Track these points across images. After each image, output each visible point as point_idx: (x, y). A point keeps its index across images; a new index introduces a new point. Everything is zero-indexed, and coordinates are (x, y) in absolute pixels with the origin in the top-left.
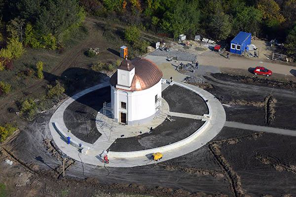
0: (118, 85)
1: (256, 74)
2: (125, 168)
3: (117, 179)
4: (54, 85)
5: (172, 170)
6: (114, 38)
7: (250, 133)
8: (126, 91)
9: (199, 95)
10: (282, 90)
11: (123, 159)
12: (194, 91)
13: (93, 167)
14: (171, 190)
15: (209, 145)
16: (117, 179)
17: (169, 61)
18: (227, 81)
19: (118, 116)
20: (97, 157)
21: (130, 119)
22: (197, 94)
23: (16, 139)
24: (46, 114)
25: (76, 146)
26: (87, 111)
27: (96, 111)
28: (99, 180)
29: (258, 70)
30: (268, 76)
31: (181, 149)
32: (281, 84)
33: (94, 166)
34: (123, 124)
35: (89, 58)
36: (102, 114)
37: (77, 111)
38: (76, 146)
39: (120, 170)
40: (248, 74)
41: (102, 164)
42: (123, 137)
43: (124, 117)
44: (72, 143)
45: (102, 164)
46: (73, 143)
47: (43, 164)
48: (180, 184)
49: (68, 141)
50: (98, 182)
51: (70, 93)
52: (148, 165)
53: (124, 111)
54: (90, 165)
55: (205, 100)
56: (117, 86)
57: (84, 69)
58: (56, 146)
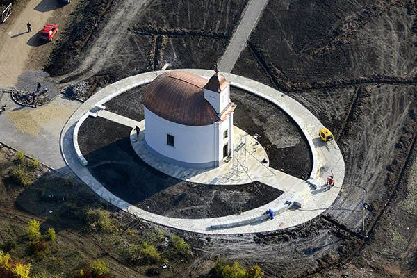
7: (252, 47)
25: (282, 210)
44: (278, 213)
49: (270, 215)
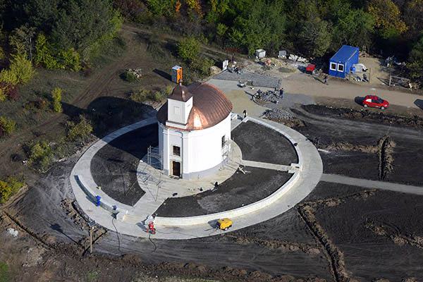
0: (169, 122)
1: (366, 106)
2: (178, 240)
3: (167, 256)
4: (77, 121)
5: (245, 244)
6: (163, 55)
7: (357, 191)
8: (180, 130)
9: (284, 136)
10: (403, 129)
11: (175, 228)
12: (277, 130)
13: (133, 239)
14: (244, 272)
15: (299, 208)
16: (167, 256)
17: (241, 87)
18: (324, 115)
19: (168, 167)
20: (139, 225)
21: (186, 170)
22: (281, 135)
23: (22, 199)
24: (65, 163)
25: (108, 209)
26: (125, 159)
27: (137, 159)
28: (141, 258)
29: (369, 100)
30: (383, 108)
31: (259, 213)
32: (401, 120)
33: (135, 237)
34: (175, 178)
35: (127, 83)
36: (145, 164)
37: (110, 160)
38: (108, 209)
39: (172, 243)
40: (355, 106)
41: (146, 235)
42: (176, 196)
43: (177, 167)
44: (102, 205)
45: (146, 235)
46: (105, 205)
47: (62, 235)
48: (257, 263)
49: (97, 202)
50: (140, 260)
51: (99, 134)
52: (211, 237)
53: (177, 159)
54: (128, 236)
55: (294, 143)
56: (167, 124)
57: (121, 99)
58: (80, 208)
